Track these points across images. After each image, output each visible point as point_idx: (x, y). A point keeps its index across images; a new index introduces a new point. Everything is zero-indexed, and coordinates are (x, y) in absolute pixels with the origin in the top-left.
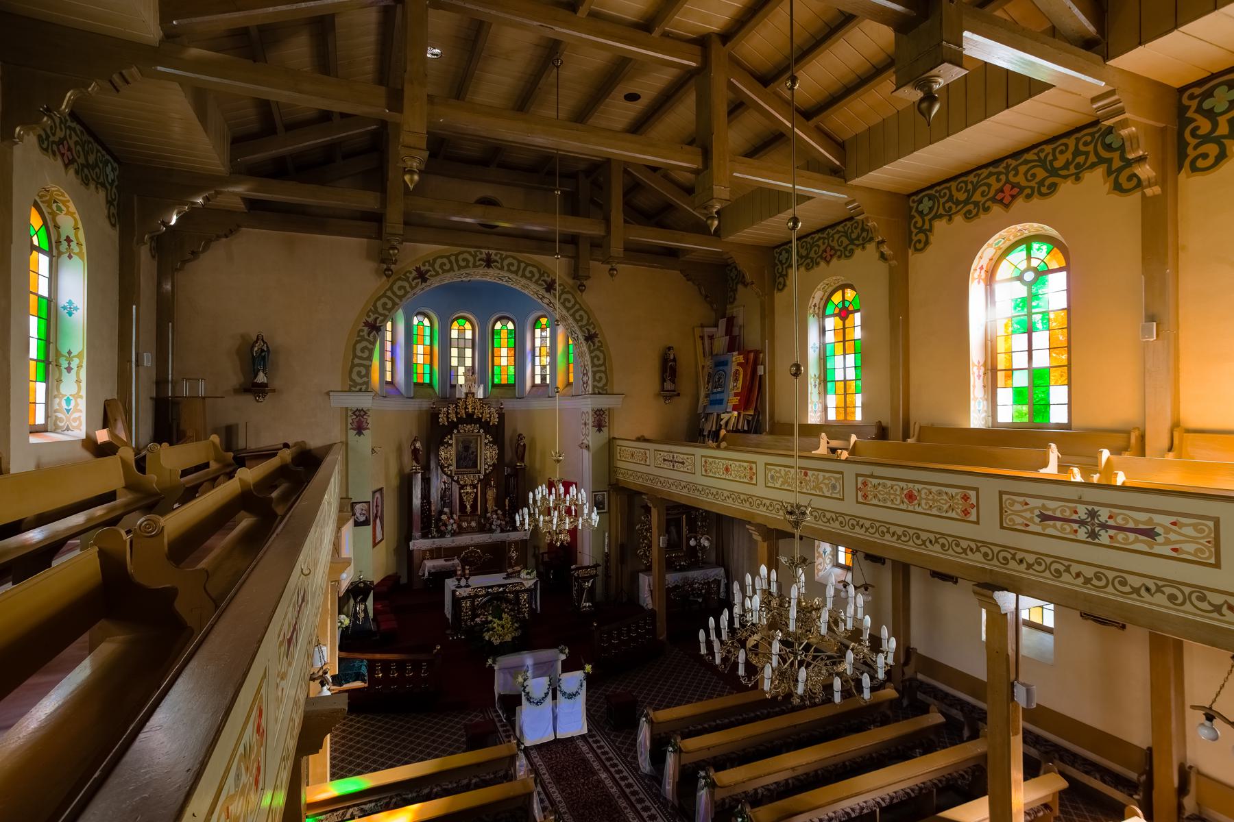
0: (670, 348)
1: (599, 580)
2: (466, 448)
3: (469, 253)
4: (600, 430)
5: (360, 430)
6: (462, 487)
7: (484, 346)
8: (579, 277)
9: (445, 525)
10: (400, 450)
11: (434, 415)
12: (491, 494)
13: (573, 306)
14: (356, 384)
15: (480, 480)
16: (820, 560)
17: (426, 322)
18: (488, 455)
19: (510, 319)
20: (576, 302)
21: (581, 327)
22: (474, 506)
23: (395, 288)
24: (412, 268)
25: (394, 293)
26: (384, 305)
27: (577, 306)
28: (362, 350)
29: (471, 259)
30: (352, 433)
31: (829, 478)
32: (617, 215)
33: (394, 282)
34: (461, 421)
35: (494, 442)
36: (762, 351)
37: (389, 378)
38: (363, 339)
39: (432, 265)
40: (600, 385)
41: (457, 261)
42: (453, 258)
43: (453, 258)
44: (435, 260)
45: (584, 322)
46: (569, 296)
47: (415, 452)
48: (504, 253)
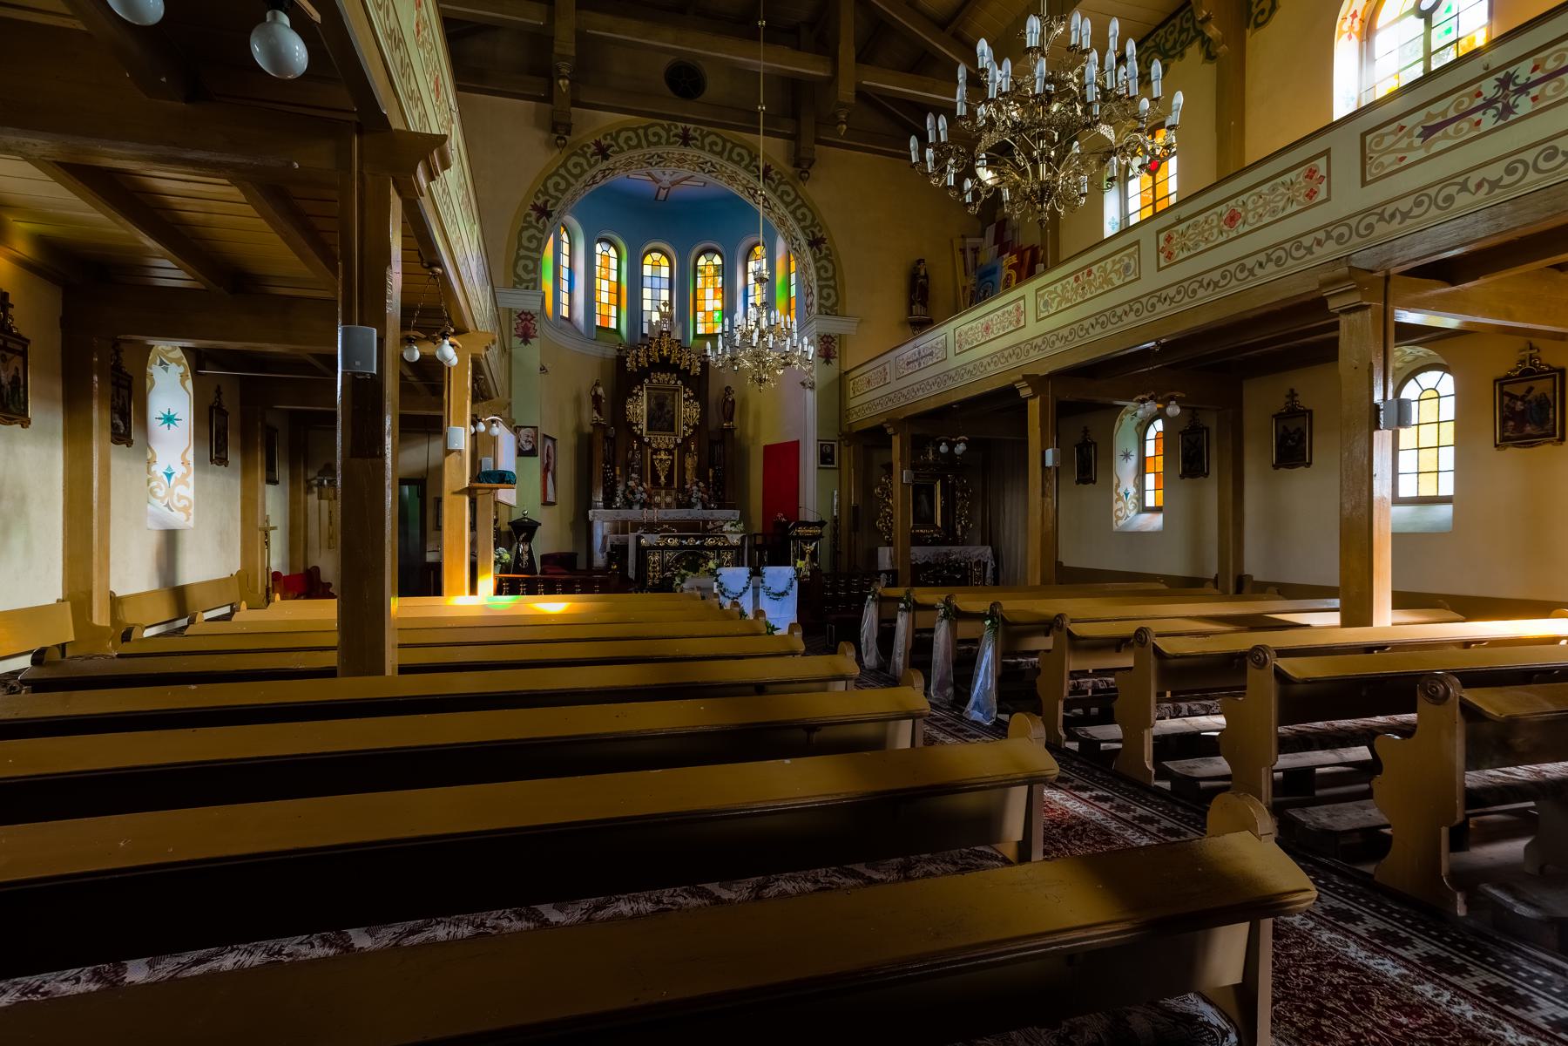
0: (920, 261)
1: (826, 540)
2: (661, 406)
3: (662, 126)
4: (827, 362)
5: (526, 337)
6: (656, 451)
7: (683, 286)
8: (802, 164)
9: (633, 492)
10: (578, 400)
11: (620, 360)
12: (690, 462)
13: (794, 201)
14: (521, 281)
15: (677, 445)
16: (1120, 504)
17: (612, 252)
18: (687, 412)
19: (715, 252)
20: (797, 196)
21: (803, 229)
22: (669, 477)
23: (570, 165)
24: (590, 141)
25: (568, 171)
26: (557, 185)
27: (799, 202)
28: (530, 239)
29: (663, 133)
30: (517, 341)
31: (1121, 260)
32: (847, 52)
33: (568, 158)
34: (654, 367)
35: (696, 398)
36: (1044, 247)
37: (565, 314)
38: (530, 226)
39: (615, 139)
40: (828, 304)
41: (646, 135)
42: (641, 132)
43: (641, 132)
44: (618, 133)
45: (808, 222)
46: (788, 188)
47: (596, 399)
48: (706, 129)
